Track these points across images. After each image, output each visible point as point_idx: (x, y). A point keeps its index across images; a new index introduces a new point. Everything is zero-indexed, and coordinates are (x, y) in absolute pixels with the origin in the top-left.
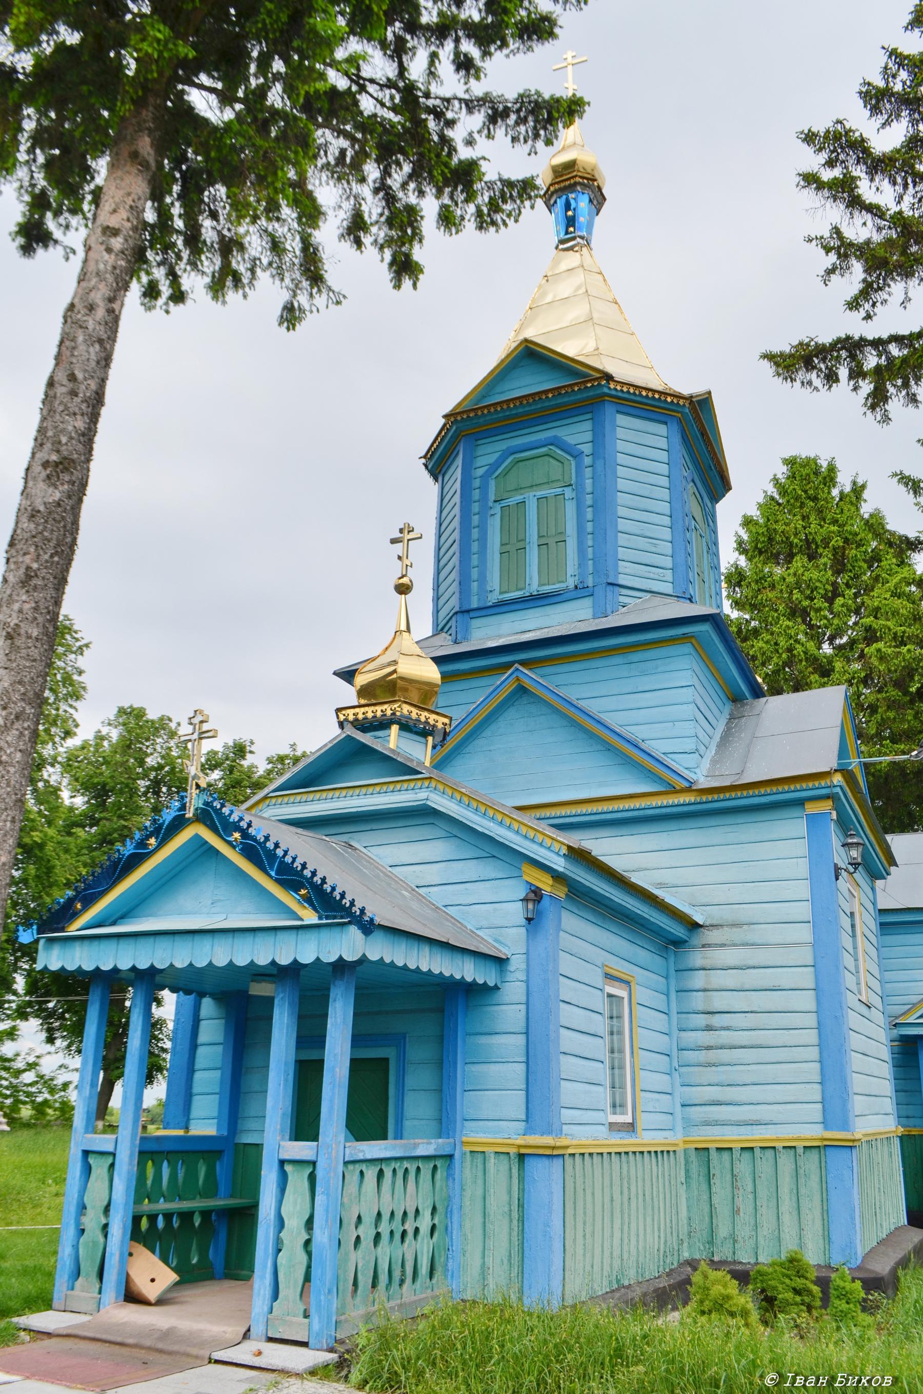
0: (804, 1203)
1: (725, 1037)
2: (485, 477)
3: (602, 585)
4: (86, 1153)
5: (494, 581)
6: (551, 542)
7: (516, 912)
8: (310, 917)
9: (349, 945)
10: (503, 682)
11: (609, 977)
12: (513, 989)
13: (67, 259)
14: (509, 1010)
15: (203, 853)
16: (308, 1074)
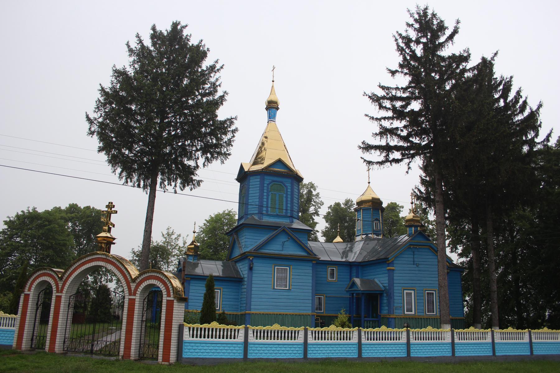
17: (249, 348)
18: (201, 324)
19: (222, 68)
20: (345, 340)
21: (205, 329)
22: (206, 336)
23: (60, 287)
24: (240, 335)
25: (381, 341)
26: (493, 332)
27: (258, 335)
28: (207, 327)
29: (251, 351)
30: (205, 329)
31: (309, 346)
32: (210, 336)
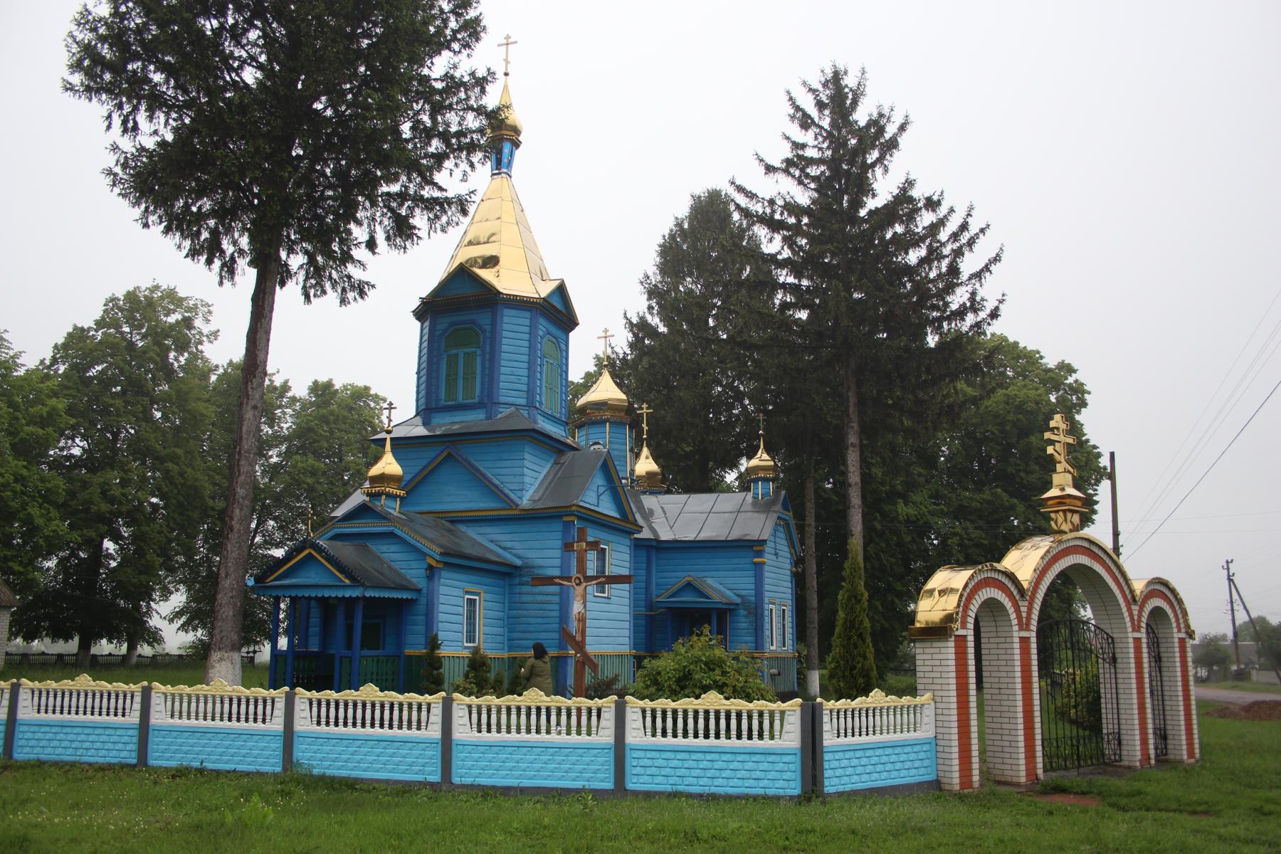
3: (488, 402)
5: (443, 395)
6: (469, 376)
7: (422, 572)
8: (347, 581)
12: (423, 601)
13: (221, 283)
14: (421, 608)
16: (350, 629)
17: (18, 735)
18: (402, 693)
19: (902, 128)
20: (251, 723)
21: (509, 709)
22: (745, 733)
23: (1024, 615)
24: (787, 727)
25: (494, 734)
26: (146, 693)
27: (483, 722)
28: (691, 708)
29: (22, 742)
30: (685, 712)
31: (23, 728)
32: (755, 733)
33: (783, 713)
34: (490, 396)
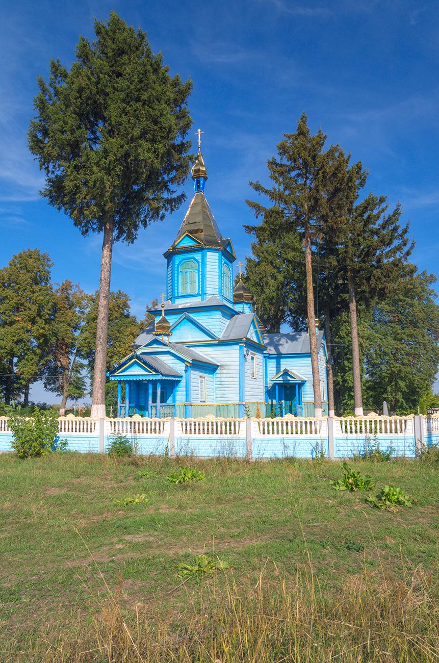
0: (236, 414)
1: (223, 386)
2: (178, 265)
3: (202, 294)
4: (120, 407)
5: (180, 291)
8: (154, 373)
9: (159, 377)
10: (183, 315)
11: (200, 377)
15: (136, 363)
16: (154, 394)
33: (406, 421)
34: (203, 291)
